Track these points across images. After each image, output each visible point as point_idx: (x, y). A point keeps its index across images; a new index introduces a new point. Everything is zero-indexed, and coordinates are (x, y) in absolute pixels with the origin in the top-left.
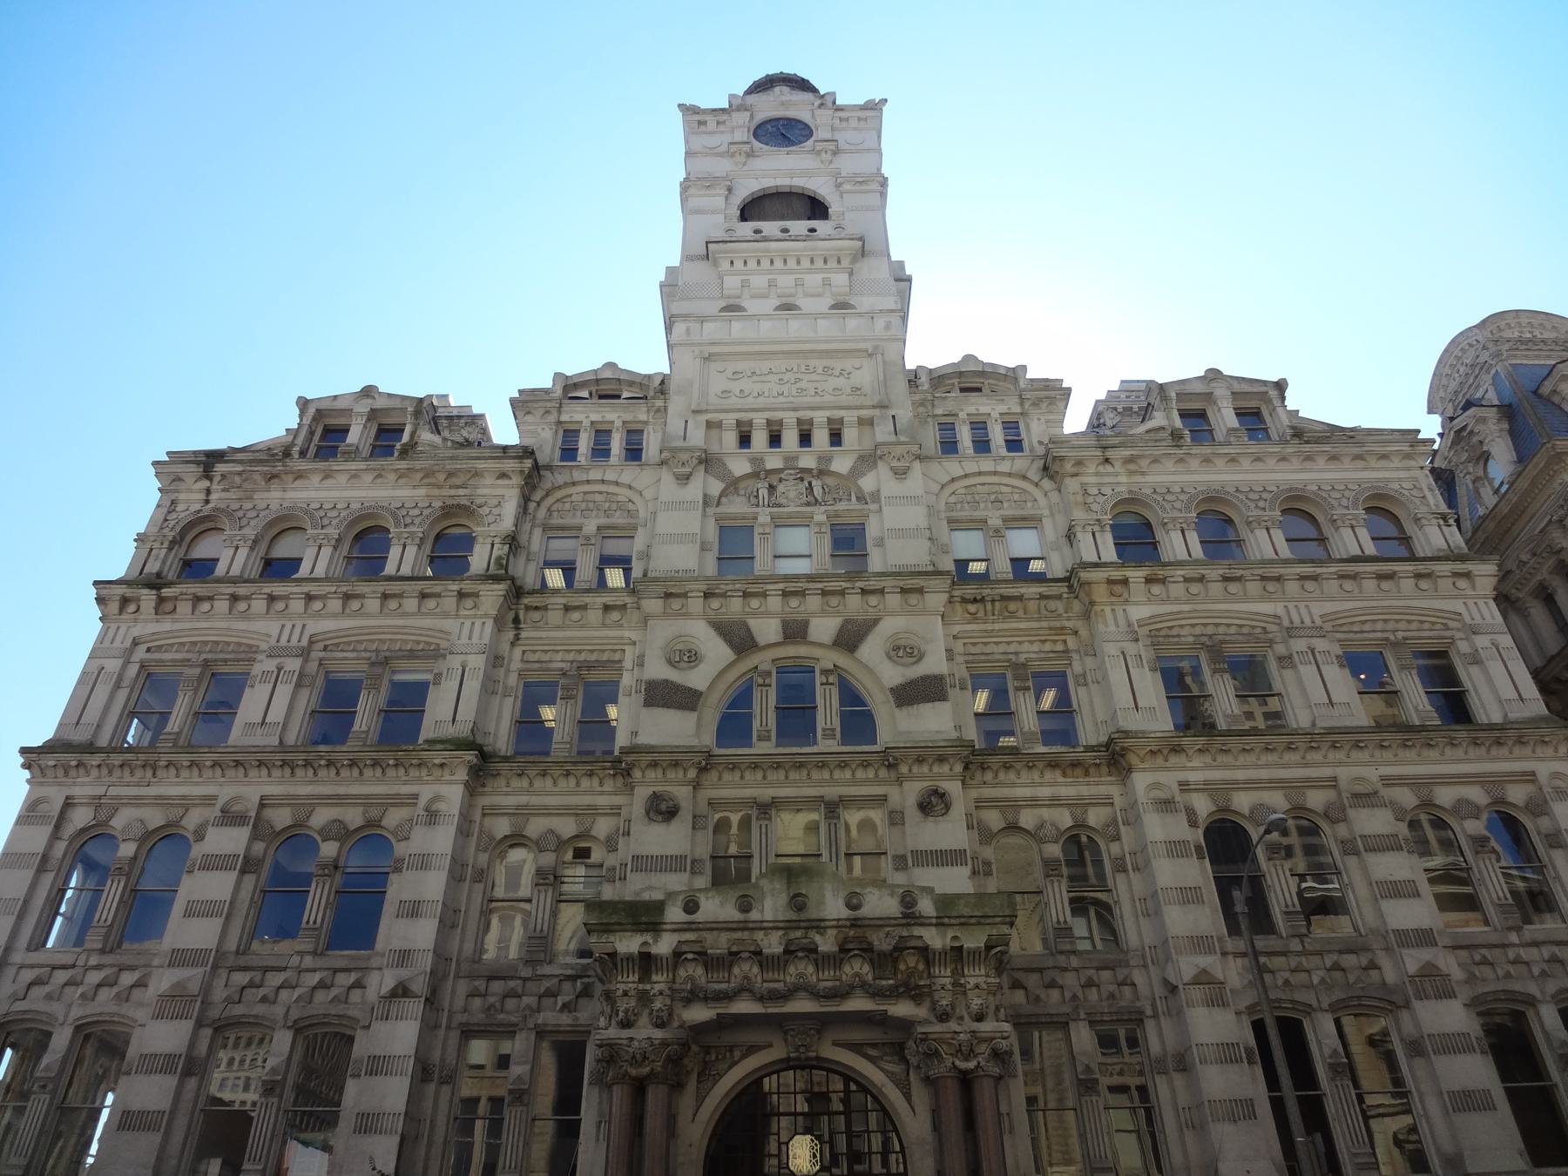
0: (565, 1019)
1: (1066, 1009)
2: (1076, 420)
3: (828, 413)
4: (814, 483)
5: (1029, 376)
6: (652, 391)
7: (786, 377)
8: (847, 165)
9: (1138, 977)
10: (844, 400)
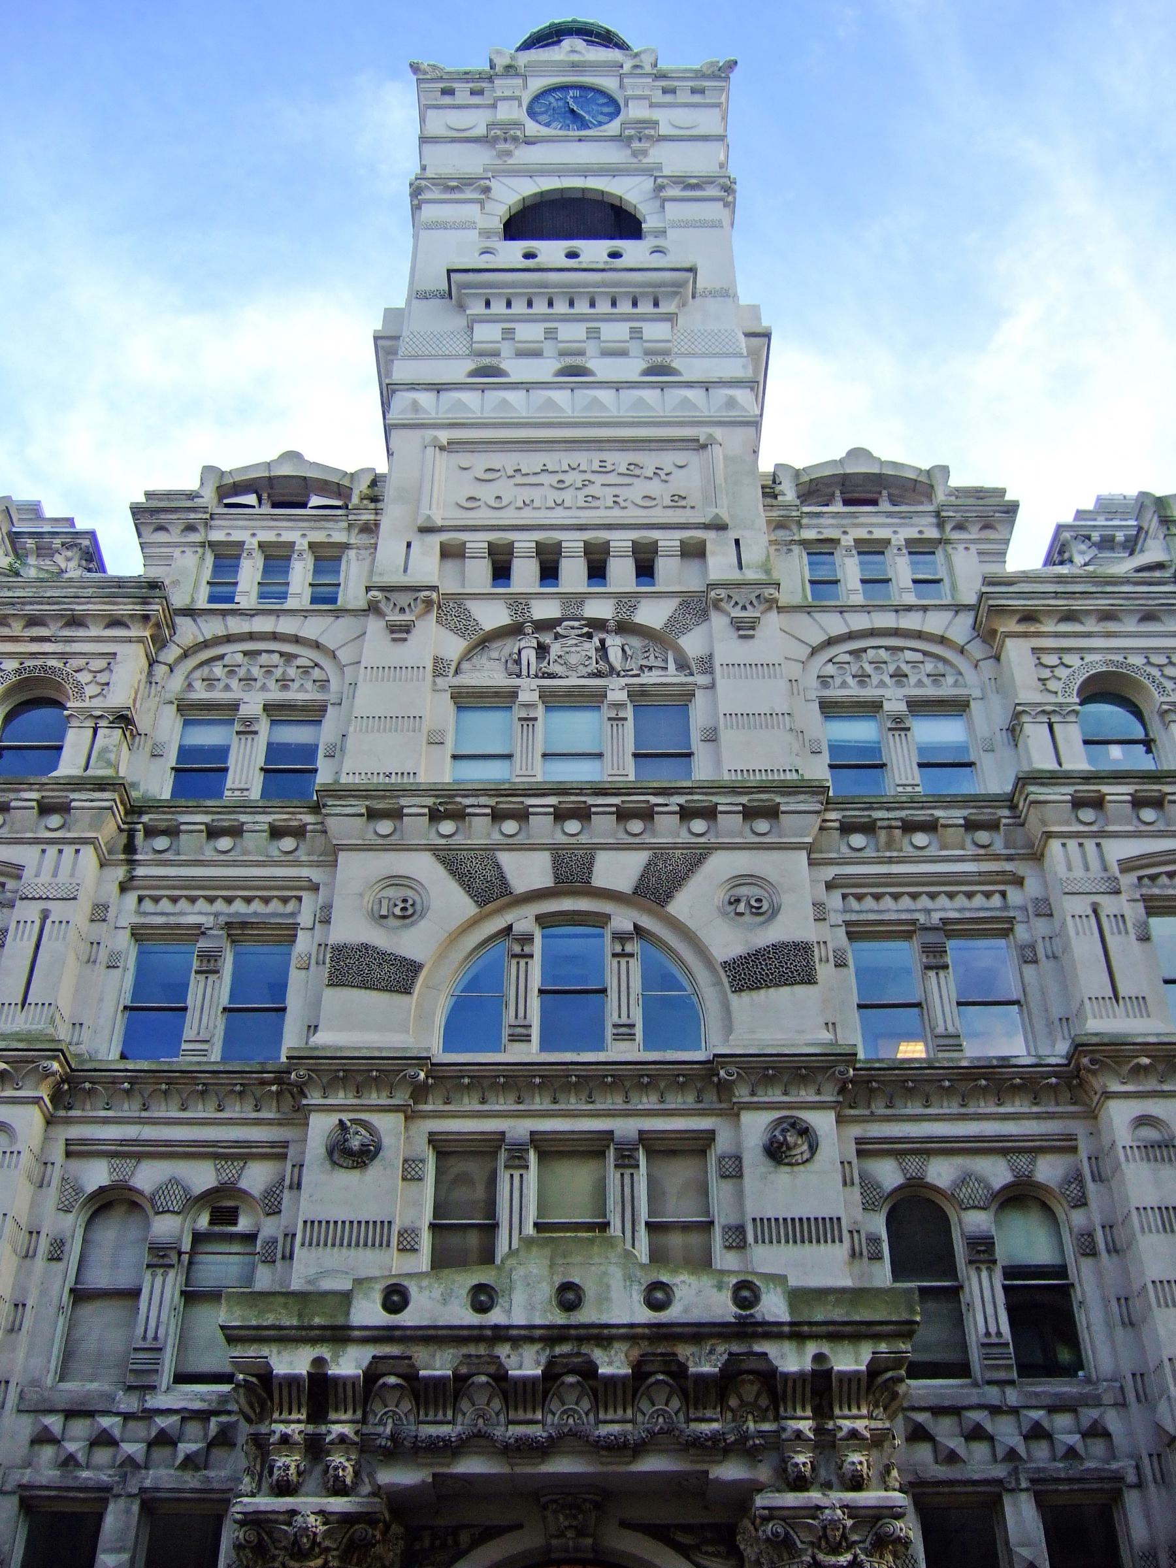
0: (192, 1480)
1: (999, 1471)
2: (1026, 552)
3: (635, 535)
4: (608, 642)
5: (955, 481)
6: (353, 501)
7: (569, 478)
8: (673, 159)
9: (1113, 1421)
10: (660, 515)
